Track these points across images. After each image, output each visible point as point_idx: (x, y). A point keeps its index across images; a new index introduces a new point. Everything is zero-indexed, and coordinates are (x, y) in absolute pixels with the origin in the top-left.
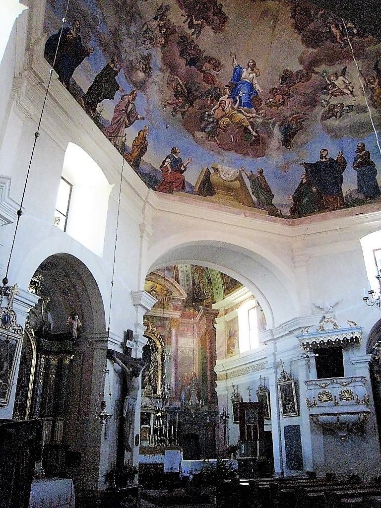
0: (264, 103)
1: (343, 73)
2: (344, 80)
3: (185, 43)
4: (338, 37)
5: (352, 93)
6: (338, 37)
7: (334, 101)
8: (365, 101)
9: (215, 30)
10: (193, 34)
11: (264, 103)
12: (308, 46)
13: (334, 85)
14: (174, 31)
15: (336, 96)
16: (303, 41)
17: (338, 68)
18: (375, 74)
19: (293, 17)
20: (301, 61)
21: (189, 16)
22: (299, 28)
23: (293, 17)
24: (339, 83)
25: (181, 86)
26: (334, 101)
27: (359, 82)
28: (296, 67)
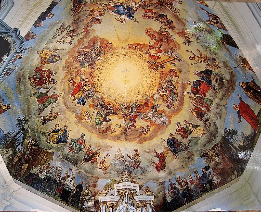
0: (106, 8)
1: (70, 43)
2: (67, 41)
3: (169, 24)
4: (84, 50)
5: (59, 41)
6: (84, 50)
7: (66, 32)
8: (51, 46)
9: (151, 29)
10: (165, 29)
11: (106, 8)
12: (95, 37)
13: (70, 36)
14: (179, 33)
15: (66, 34)
16: (98, 37)
17: (74, 43)
18: (56, 54)
19: (111, 44)
20: (94, 30)
21: (170, 37)
22: (104, 41)
23: (111, 44)
24: (69, 39)
25: (168, 6)
26: (66, 32)
27: (59, 46)
28: (95, 26)
